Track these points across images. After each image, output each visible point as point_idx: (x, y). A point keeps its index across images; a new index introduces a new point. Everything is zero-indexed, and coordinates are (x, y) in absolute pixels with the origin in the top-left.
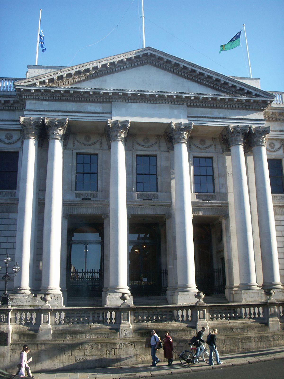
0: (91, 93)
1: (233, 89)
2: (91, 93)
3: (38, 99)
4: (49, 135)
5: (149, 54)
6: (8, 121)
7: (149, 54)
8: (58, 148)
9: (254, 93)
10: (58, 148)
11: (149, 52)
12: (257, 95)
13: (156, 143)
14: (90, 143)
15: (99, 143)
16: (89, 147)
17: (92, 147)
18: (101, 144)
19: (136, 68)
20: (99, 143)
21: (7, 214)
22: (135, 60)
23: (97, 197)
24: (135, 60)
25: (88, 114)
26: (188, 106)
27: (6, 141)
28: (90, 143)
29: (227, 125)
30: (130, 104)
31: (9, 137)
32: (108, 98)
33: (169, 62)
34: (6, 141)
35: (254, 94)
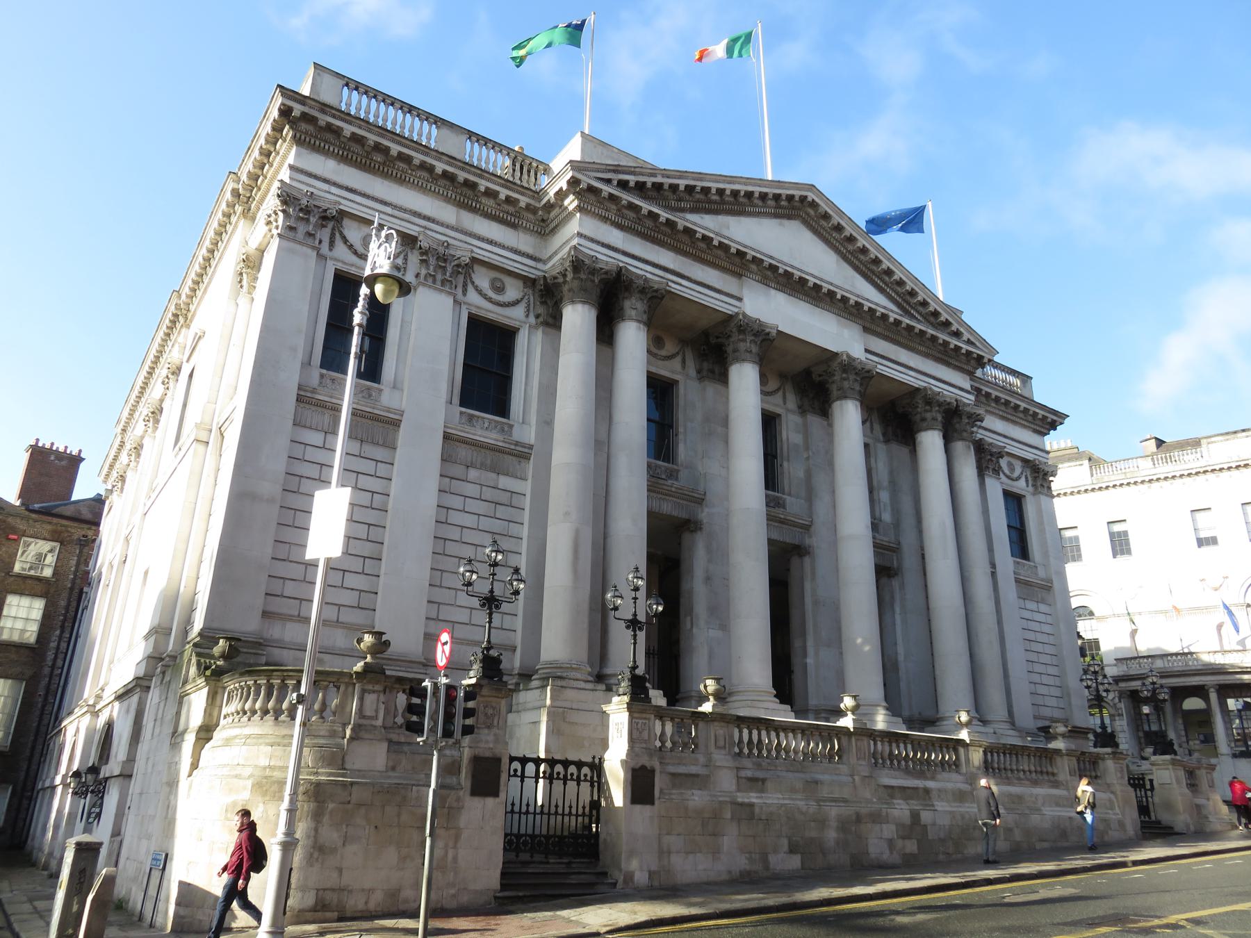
0: (715, 243)
1: (932, 319)
2: (715, 243)
3: (605, 219)
4: (622, 309)
5: (810, 199)
6: (503, 247)
7: (810, 199)
8: (632, 338)
9: (966, 336)
10: (632, 338)
11: (811, 196)
12: (969, 342)
13: (778, 390)
14: (663, 353)
15: (679, 358)
16: (660, 362)
17: (667, 363)
18: (684, 362)
19: (778, 221)
20: (679, 358)
21: (494, 475)
22: (756, 201)
23: (677, 479)
24: (756, 201)
25: (704, 287)
26: (866, 330)
27: (491, 294)
28: (663, 353)
29: (547, 422)
30: (773, 292)
31: (500, 289)
32: (740, 263)
33: (839, 228)
34: (491, 294)
35: (965, 338)
